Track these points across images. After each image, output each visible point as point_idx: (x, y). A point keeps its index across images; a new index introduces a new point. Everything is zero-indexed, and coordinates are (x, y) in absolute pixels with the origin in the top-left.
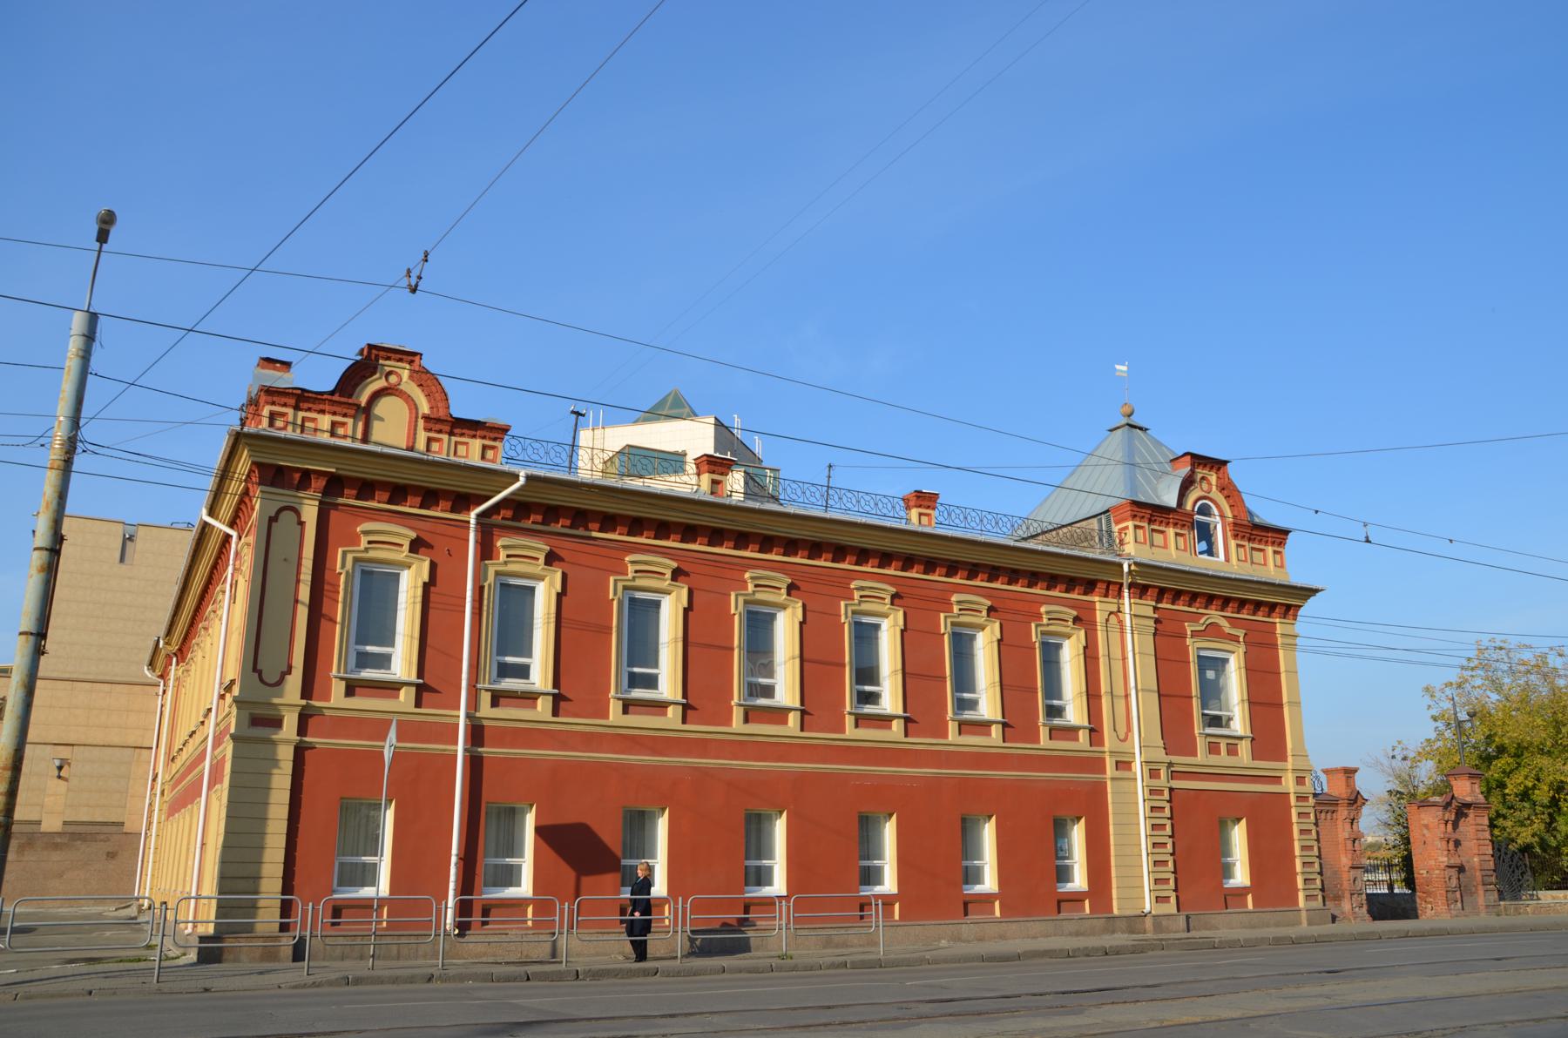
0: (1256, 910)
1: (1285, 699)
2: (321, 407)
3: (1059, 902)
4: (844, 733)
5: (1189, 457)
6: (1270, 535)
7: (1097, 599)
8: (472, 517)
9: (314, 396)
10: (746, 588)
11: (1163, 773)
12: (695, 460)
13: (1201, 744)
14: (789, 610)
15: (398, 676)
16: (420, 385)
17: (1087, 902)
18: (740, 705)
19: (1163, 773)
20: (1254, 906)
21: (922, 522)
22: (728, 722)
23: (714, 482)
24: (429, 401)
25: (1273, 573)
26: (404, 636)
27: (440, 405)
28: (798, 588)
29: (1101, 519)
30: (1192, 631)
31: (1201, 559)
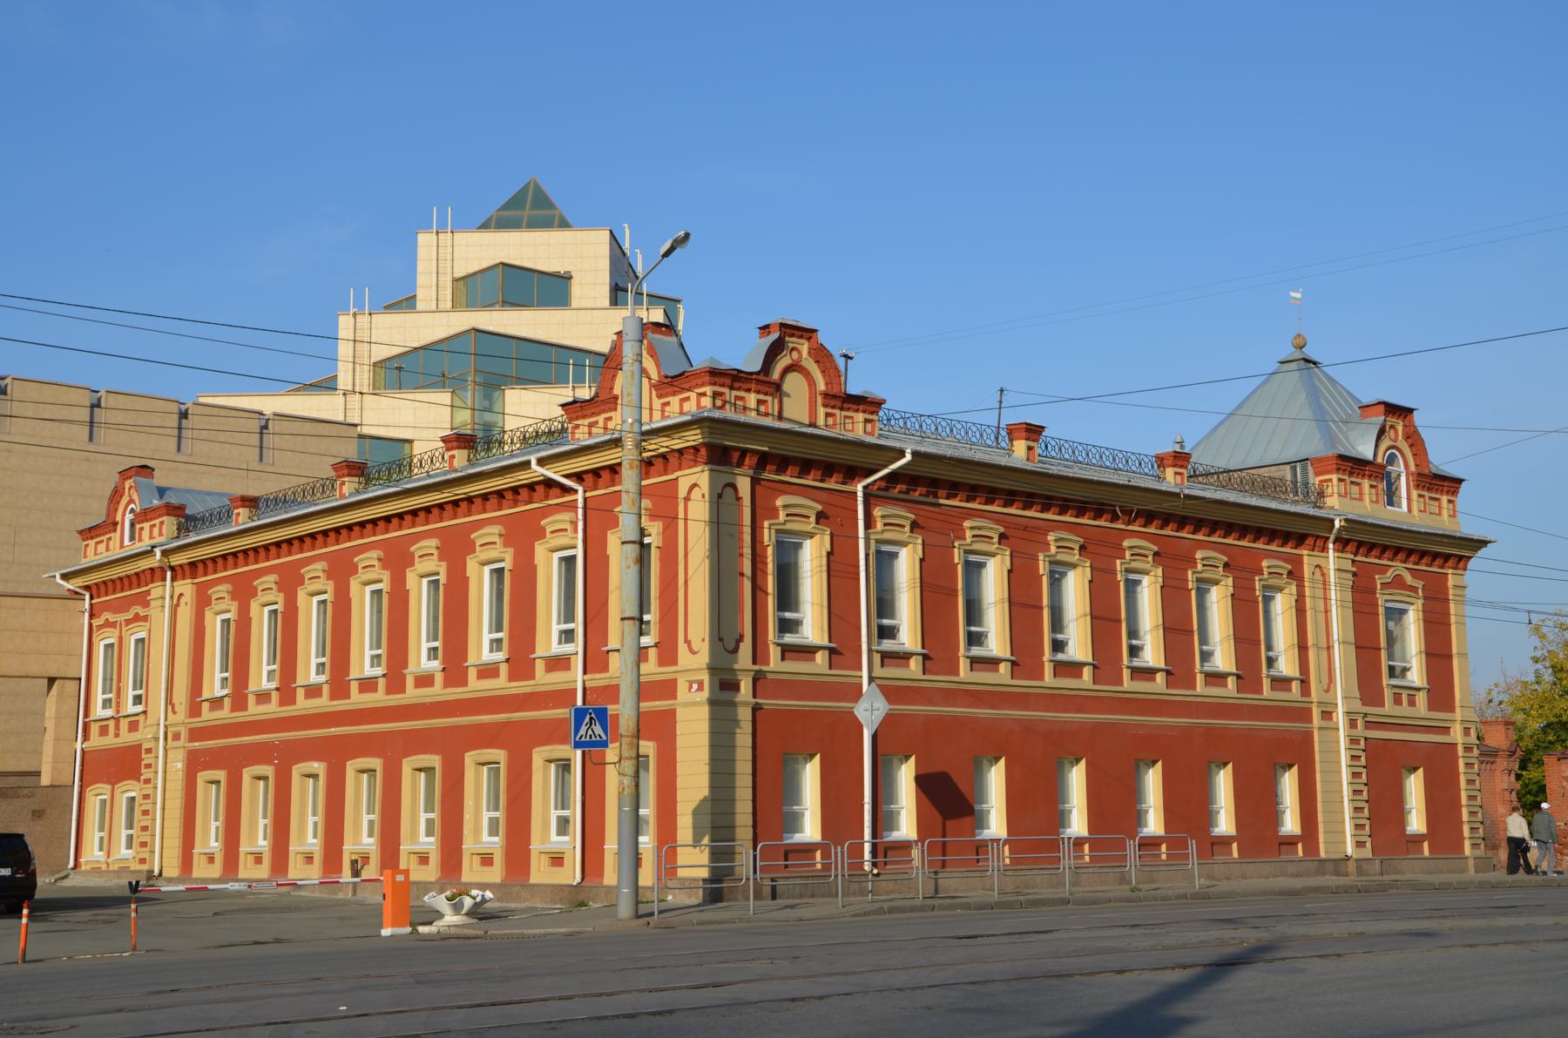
0: (1432, 857)
1: (1454, 651)
2: (747, 386)
3: (1280, 844)
4: (1263, 694)
5: (1383, 406)
6: (1446, 484)
7: (1305, 552)
8: (859, 488)
9: (745, 376)
10: (1049, 550)
11: (1360, 723)
12: (1007, 425)
13: (1388, 695)
14: (1079, 570)
15: (810, 639)
16: (817, 362)
17: (1300, 846)
18: (1051, 661)
19: (1360, 723)
20: (1430, 852)
21: (829, 423)
22: (1041, 677)
23: (1030, 448)
24: (824, 377)
25: (1447, 523)
26: (812, 604)
27: (834, 381)
28: (827, 518)
29: (1295, 467)
30: (1381, 583)
31: (1389, 510)
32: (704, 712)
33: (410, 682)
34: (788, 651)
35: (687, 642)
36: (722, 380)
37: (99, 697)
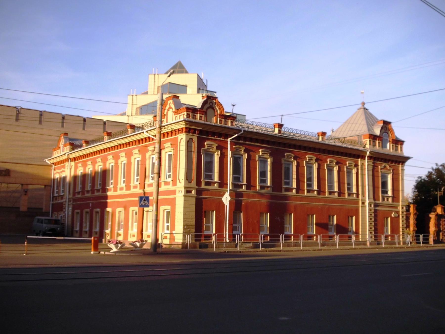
0: (244, 242)
23: (322, 138)
32: (182, 198)
33: (118, 189)
34: (207, 184)
35: (179, 180)
36: (190, 111)
37: (56, 191)
